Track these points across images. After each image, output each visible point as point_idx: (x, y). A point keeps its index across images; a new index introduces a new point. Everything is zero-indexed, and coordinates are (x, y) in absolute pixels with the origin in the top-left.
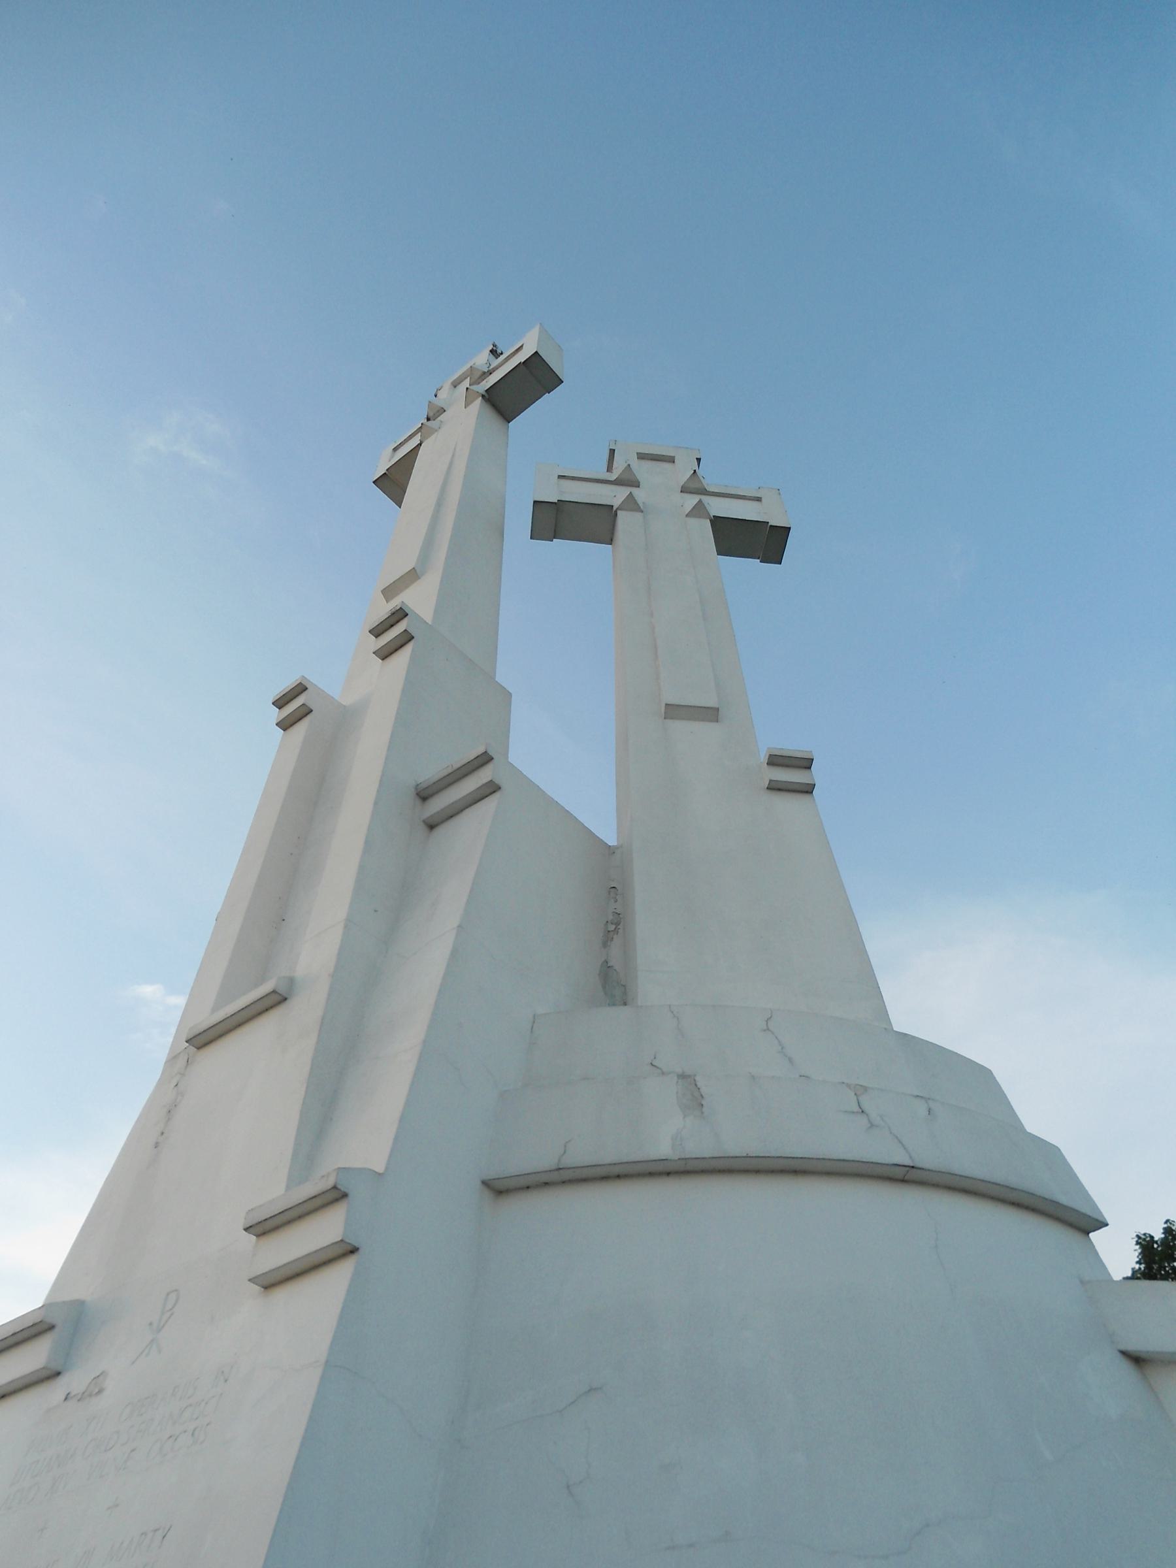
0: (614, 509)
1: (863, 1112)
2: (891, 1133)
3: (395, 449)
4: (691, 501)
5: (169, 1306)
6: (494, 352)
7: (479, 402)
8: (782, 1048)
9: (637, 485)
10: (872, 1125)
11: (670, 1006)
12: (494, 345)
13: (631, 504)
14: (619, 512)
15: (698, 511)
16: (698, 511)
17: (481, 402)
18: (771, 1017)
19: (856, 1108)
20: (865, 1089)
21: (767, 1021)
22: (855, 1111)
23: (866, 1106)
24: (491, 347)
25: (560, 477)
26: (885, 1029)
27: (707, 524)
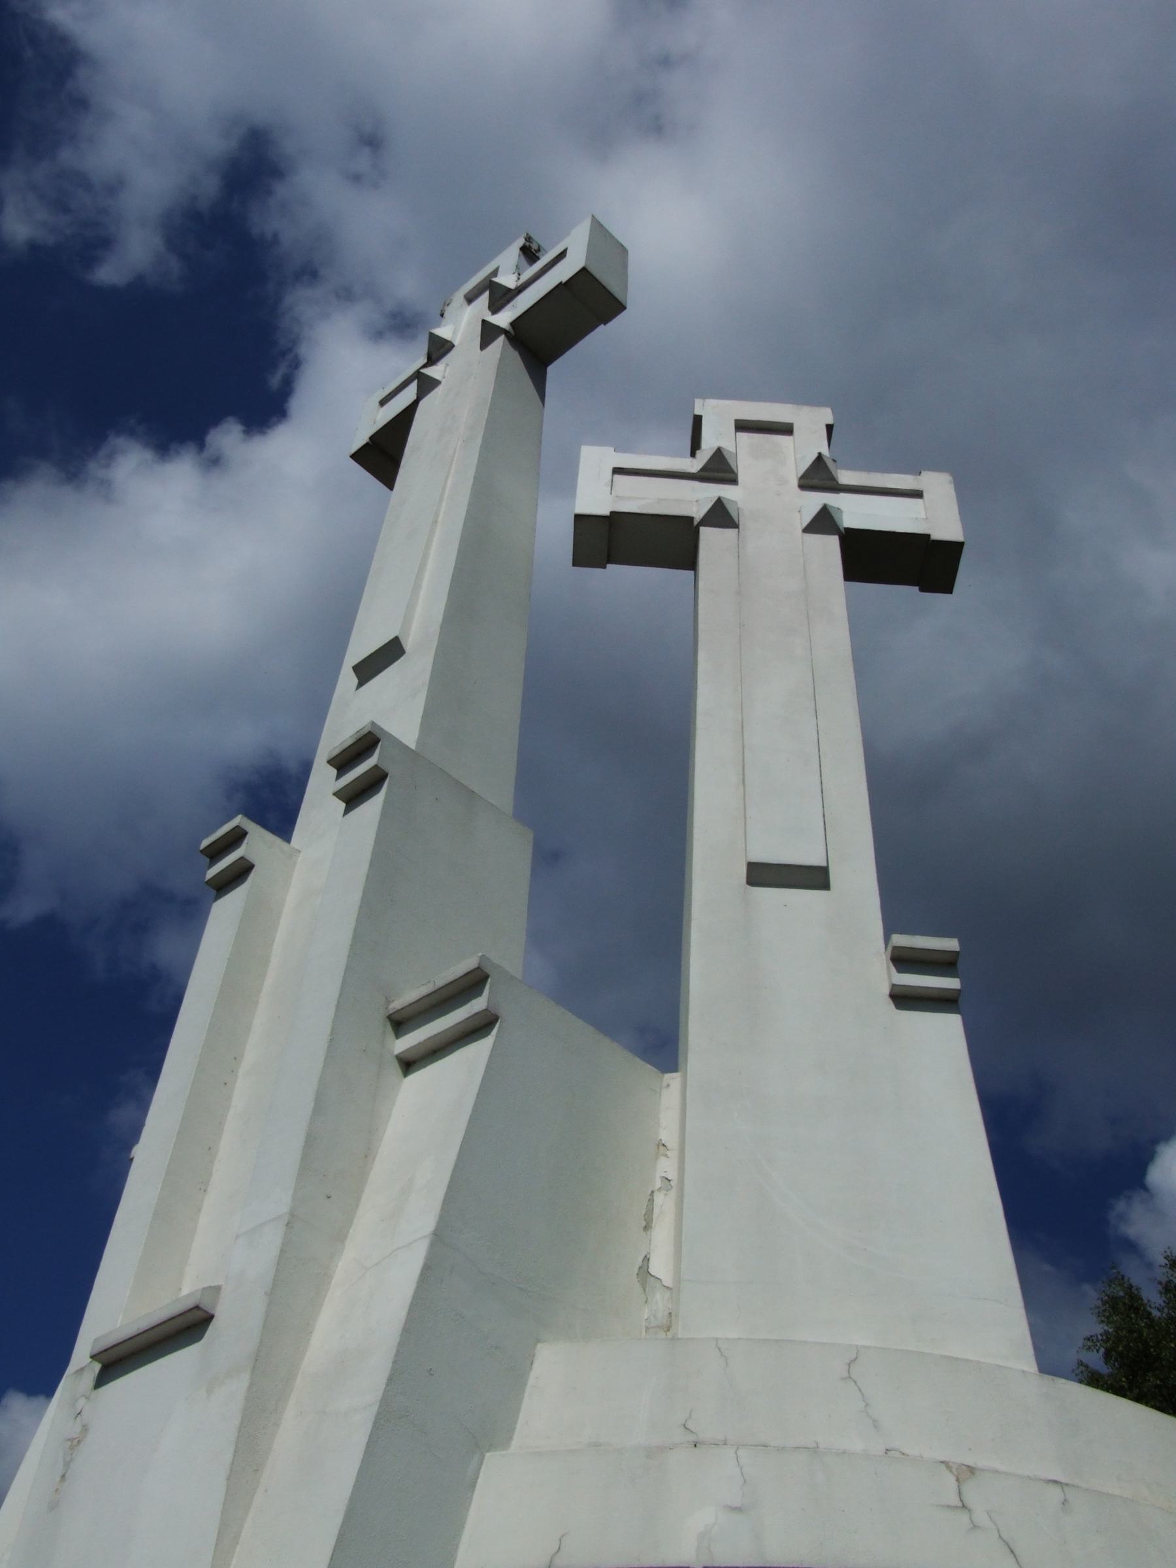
0: (696, 523)
1: (963, 1505)
2: (1000, 1537)
3: (383, 403)
4: (815, 501)
5: (410, 393)
6: (530, 253)
7: (501, 343)
8: (867, 1405)
9: (731, 478)
10: (975, 1527)
11: (717, 1339)
12: (529, 239)
13: (720, 515)
14: (703, 530)
15: (823, 522)
16: (823, 522)
17: (504, 342)
18: (856, 1358)
19: (955, 1501)
20: (971, 1470)
21: (849, 1365)
22: (953, 1504)
23: (969, 1499)
24: (521, 242)
25: (617, 471)
26: (1024, 1372)
27: (833, 542)
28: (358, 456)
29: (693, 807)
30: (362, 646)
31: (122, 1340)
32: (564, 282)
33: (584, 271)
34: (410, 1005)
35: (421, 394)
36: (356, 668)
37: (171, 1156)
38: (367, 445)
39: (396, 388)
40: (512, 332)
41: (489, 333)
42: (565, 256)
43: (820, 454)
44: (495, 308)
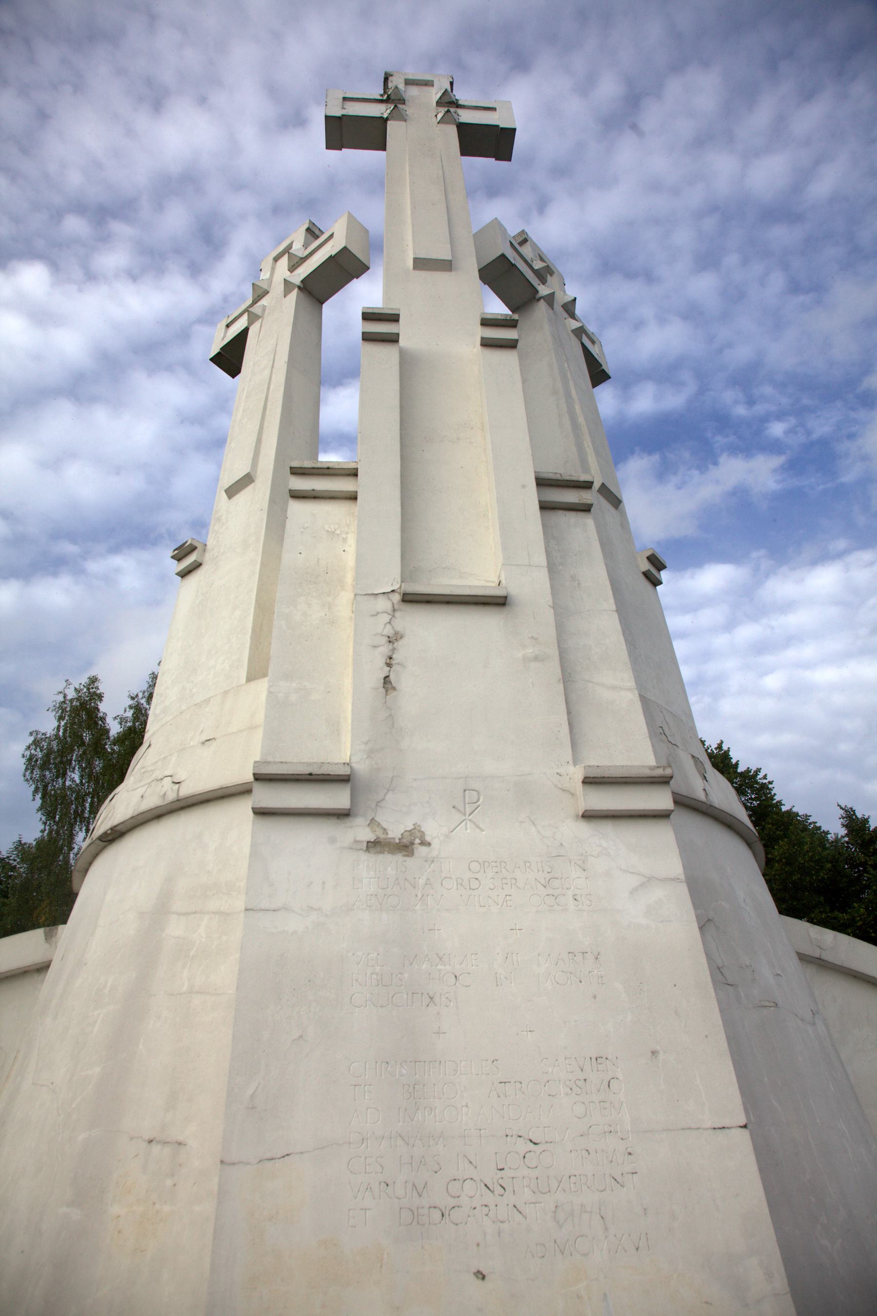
6: (312, 232)
17: (298, 293)
24: (306, 226)
28: (211, 360)
29: (614, 810)
30: (228, 479)
31: (698, 799)
32: (333, 255)
33: (345, 249)
34: (208, 792)
35: (251, 322)
36: (226, 491)
37: (352, 710)
38: (219, 353)
39: (243, 311)
40: (302, 286)
41: (288, 286)
42: (333, 237)
43: (592, 482)
44: (292, 268)
